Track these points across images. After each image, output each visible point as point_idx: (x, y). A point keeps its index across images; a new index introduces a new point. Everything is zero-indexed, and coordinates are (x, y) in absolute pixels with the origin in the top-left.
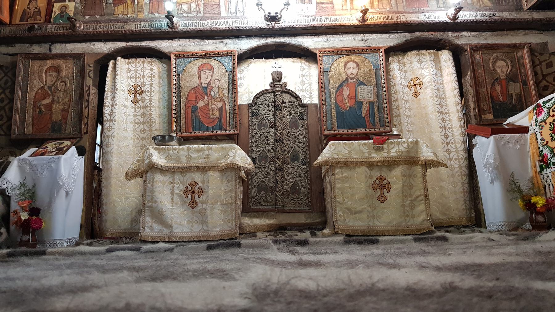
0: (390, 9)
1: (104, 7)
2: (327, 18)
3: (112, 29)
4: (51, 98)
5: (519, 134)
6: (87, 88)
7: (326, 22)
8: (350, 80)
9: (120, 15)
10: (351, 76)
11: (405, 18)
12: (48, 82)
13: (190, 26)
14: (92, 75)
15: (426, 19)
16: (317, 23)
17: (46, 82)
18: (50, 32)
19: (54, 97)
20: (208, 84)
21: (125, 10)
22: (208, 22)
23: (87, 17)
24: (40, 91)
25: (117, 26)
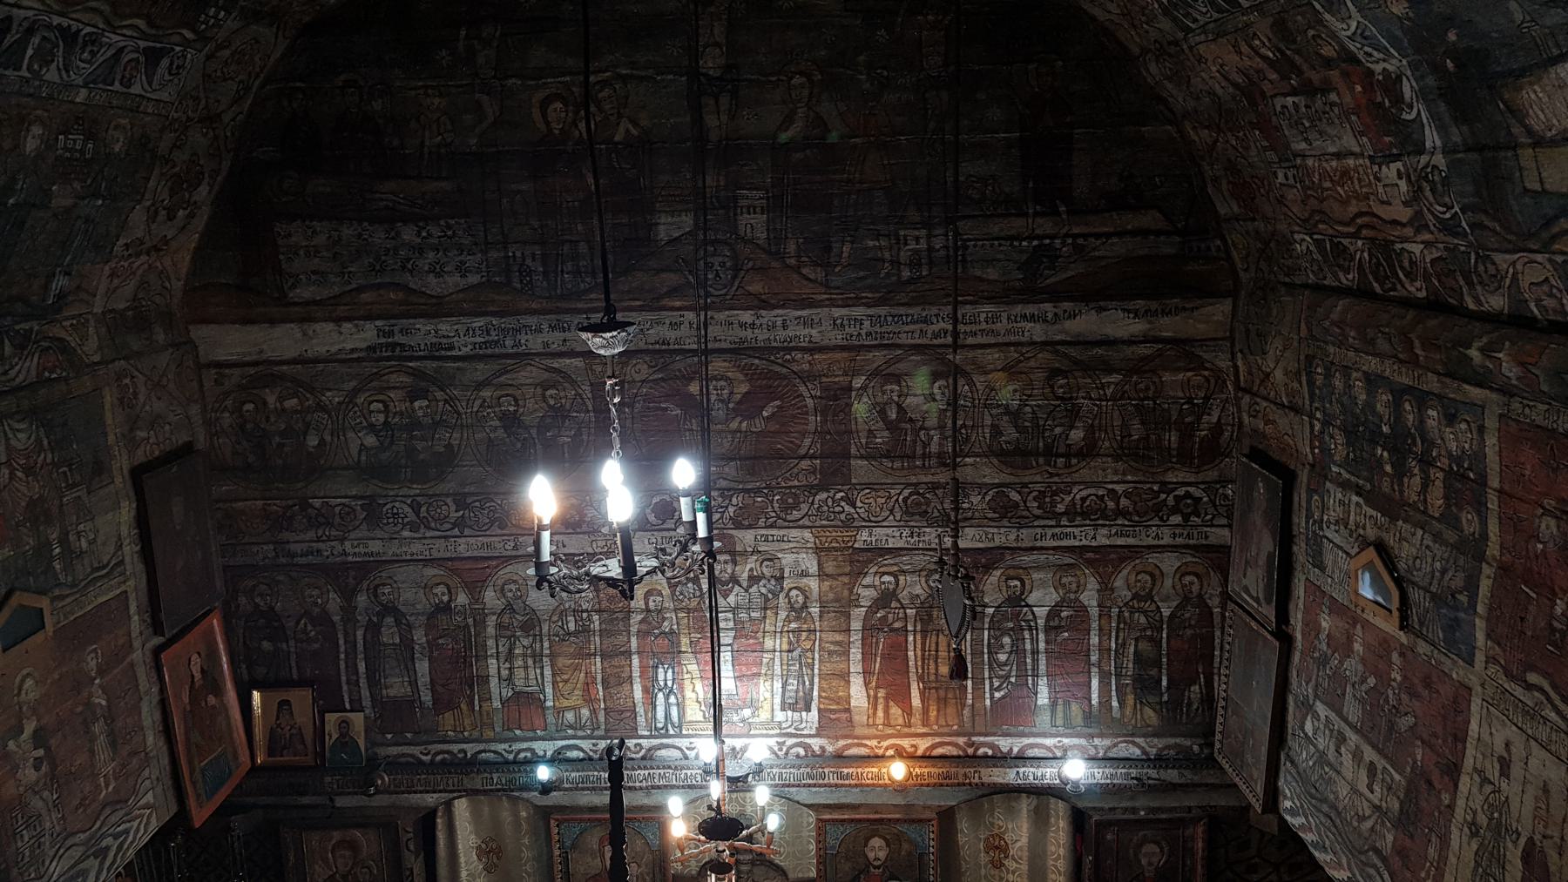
0: (959, 726)
2: (833, 773)
5: (1274, 620)
6: (408, 873)
9: (449, 733)
11: (980, 778)
13: (583, 783)
14: (412, 847)
15: (1019, 781)
23: (389, 736)
25: (450, 782)
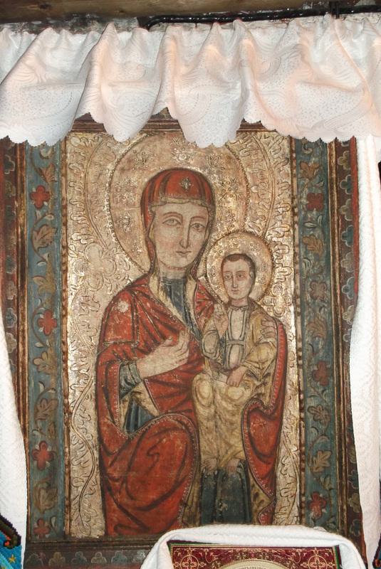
4: (183, 341)
24: (124, 306)
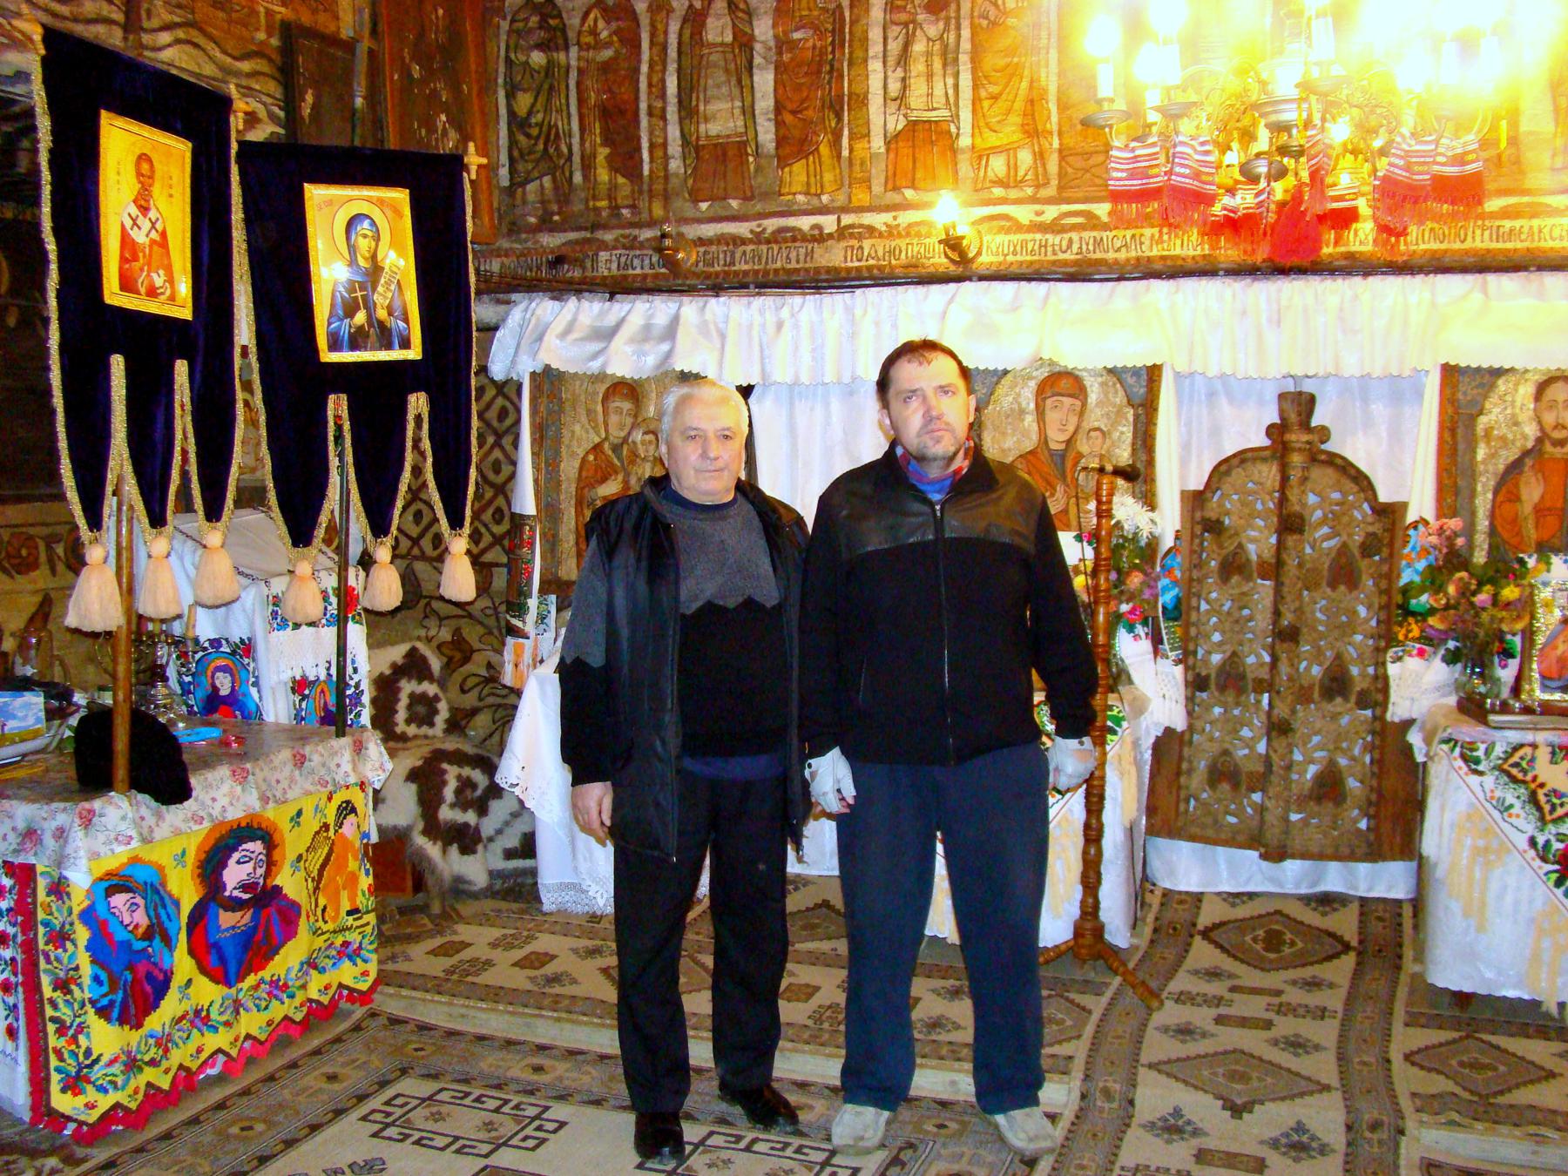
1: (752, 167)
3: (779, 265)
4: (620, 477)
7: (1478, 244)
8: (1548, 448)
10: (1557, 435)
12: (611, 430)
16: (1444, 246)
17: (607, 431)
18: (606, 273)
19: (627, 474)
20: (1069, 442)
21: (812, 180)
22: (1071, 241)
23: (704, 206)
24: (591, 458)
25: (793, 255)
